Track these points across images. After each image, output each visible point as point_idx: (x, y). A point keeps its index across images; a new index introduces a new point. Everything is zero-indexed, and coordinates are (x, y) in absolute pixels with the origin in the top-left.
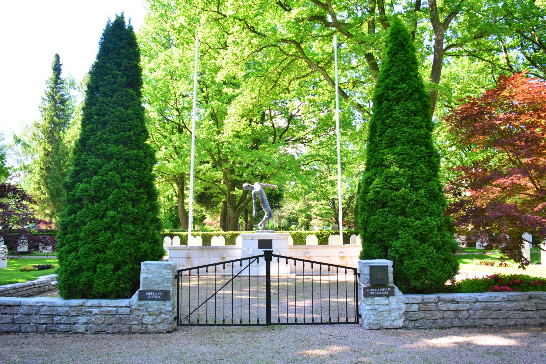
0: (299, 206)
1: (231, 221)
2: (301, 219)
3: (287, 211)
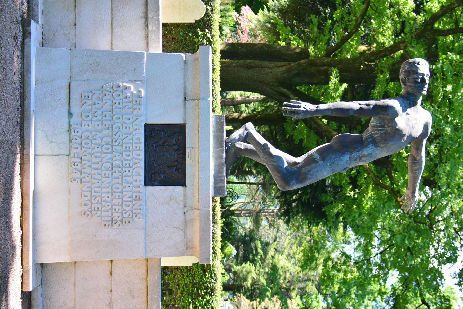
0: (288, 266)
1: (250, 72)
2: (252, 272)
3: (272, 233)
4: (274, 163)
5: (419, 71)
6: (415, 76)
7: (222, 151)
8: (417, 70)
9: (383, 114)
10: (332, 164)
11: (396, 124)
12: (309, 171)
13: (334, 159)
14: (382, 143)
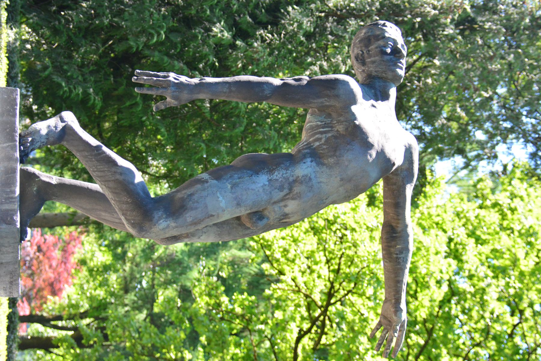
4: (118, 177)
5: (387, 35)
6: (381, 43)
7: (13, 148)
8: (384, 34)
9: (328, 96)
10: (234, 186)
11: (353, 117)
12: (191, 195)
13: (239, 178)
14: (331, 157)
